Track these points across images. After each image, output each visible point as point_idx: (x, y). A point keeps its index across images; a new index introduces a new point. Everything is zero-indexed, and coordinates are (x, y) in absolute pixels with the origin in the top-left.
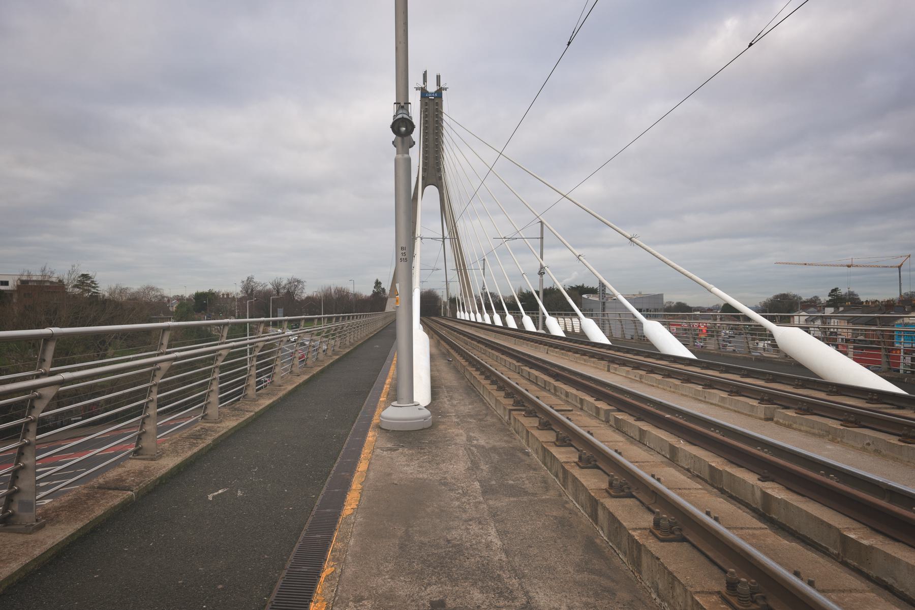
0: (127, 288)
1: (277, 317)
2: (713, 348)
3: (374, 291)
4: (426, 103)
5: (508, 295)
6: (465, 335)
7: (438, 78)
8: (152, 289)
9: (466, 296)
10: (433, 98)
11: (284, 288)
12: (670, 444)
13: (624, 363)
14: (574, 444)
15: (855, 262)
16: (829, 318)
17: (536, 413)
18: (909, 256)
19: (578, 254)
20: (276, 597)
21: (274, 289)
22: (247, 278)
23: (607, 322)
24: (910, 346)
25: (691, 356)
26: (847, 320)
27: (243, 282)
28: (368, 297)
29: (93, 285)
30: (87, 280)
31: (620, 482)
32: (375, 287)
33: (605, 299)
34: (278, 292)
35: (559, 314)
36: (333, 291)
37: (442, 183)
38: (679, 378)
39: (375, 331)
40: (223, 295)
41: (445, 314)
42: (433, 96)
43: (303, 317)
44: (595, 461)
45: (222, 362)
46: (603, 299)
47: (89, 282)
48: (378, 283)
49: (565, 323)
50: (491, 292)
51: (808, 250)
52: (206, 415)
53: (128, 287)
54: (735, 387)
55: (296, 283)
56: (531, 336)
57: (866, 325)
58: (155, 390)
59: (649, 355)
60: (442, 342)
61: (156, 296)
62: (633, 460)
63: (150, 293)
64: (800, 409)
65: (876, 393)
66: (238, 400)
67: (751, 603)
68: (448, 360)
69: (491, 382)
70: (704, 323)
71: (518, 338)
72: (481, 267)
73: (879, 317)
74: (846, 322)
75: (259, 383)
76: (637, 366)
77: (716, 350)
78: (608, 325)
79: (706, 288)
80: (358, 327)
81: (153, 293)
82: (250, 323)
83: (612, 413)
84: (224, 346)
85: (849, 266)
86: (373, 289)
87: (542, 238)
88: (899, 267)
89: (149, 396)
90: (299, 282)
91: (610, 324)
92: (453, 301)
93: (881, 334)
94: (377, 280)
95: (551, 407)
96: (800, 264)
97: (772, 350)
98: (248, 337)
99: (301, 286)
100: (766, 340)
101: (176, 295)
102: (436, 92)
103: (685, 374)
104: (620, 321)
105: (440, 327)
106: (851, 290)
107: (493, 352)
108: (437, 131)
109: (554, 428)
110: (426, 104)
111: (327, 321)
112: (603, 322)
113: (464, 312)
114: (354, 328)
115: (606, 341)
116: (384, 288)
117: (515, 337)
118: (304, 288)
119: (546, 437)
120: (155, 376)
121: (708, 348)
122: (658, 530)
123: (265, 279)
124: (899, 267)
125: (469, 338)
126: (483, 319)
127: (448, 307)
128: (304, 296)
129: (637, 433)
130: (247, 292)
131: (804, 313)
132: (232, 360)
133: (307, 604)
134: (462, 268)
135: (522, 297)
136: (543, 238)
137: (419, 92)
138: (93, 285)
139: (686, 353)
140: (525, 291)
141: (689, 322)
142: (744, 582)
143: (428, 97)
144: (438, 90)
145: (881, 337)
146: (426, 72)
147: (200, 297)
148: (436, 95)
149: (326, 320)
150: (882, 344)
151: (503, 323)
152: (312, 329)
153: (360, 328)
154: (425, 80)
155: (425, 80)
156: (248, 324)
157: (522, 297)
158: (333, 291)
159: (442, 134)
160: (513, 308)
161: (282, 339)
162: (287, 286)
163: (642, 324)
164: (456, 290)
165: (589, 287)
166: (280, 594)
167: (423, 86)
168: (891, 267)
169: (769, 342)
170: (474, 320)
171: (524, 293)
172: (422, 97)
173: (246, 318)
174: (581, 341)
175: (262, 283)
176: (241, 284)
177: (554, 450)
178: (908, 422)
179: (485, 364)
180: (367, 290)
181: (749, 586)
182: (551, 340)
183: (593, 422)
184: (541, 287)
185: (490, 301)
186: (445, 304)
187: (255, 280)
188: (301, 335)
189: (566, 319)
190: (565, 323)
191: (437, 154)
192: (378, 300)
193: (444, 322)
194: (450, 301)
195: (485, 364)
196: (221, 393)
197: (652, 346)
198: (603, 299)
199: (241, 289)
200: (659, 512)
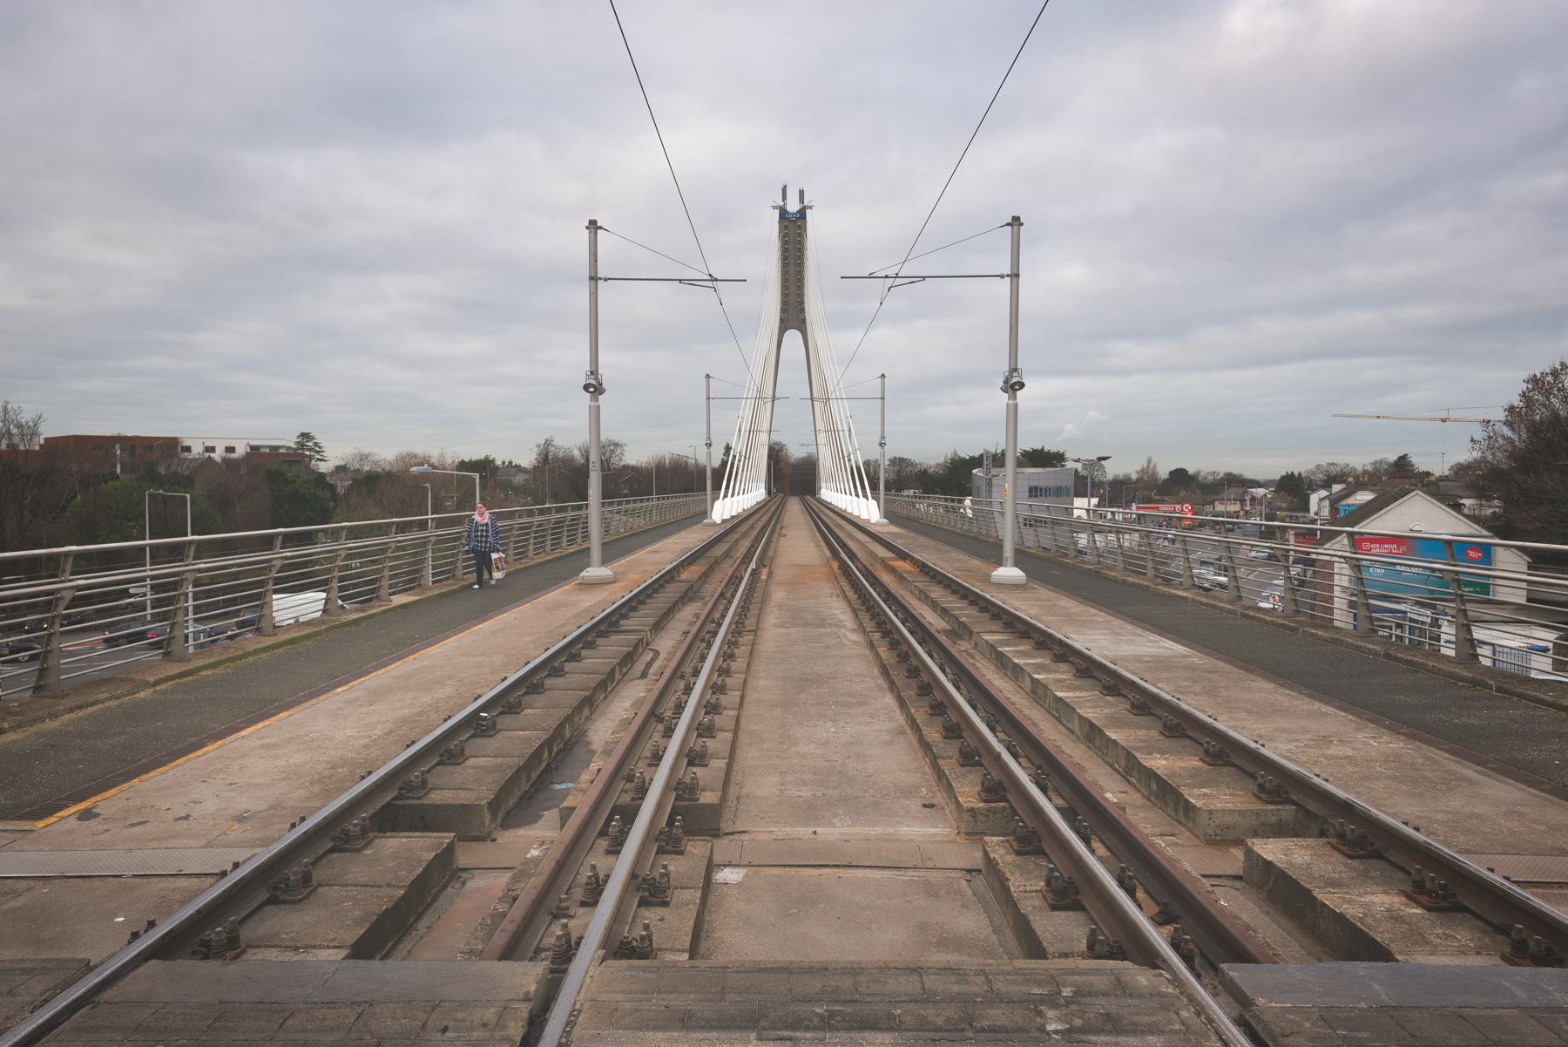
7: (802, 193)
15: (1453, 415)
21: (583, 456)
22: (544, 441)
24: (1272, 606)
27: (539, 446)
30: (308, 442)
36: (667, 461)
47: (310, 444)
53: (372, 452)
55: (612, 448)
82: (151, 546)
84: (570, 514)
85: (1444, 420)
90: (616, 445)
96: (609, 279)
98: (148, 567)
99: (619, 450)
110: (786, 227)
132: (113, 602)
136: (1017, 275)
143: (788, 218)
147: (1179, 476)
152: (272, 556)
154: (784, 198)
155: (784, 198)
156: (148, 548)
158: (667, 461)
165: (1052, 451)
167: (781, 204)
173: (187, 535)
176: (537, 449)
187: (555, 443)
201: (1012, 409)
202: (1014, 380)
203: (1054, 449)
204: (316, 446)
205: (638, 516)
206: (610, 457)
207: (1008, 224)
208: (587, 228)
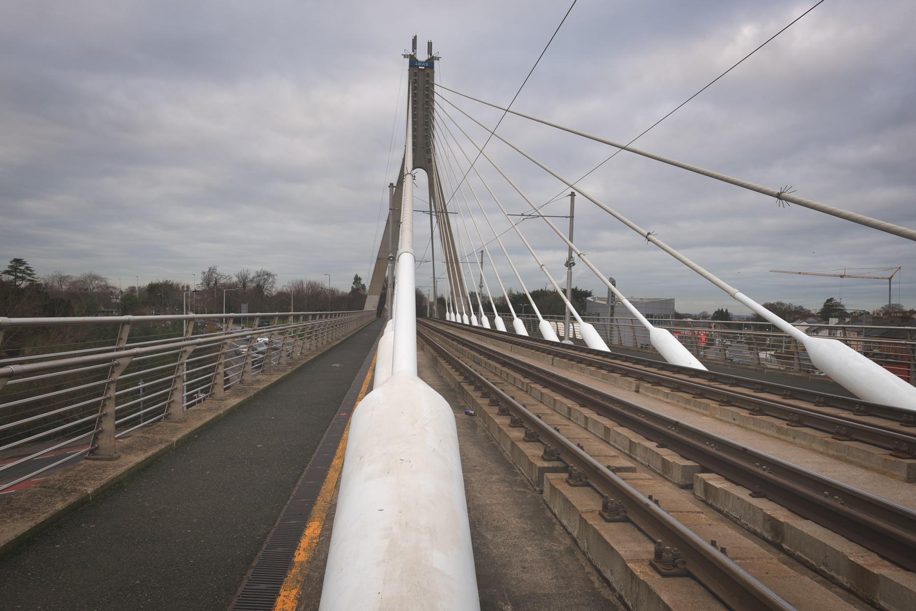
0: (68, 276)
1: (241, 313)
2: (631, 346)
3: (353, 287)
4: (416, 73)
5: (497, 296)
6: (472, 348)
7: (430, 45)
8: (96, 278)
9: (458, 296)
10: (424, 68)
11: (252, 281)
12: (605, 426)
13: (626, 373)
14: (632, 518)
15: (848, 273)
16: (834, 329)
17: (509, 411)
18: (900, 268)
19: (541, 264)
20: (246, 585)
23: (615, 329)
25: (702, 367)
26: (857, 332)
27: (204, 273)
28: (346, 294)
29: (29, 272)
30: (20, 266)
31: (616, 504)
32: (354, 283)
33: (614, 302)
34: (244, 286)
35: (551, 318)
36: (305, 286)
37: (432, 166)
38: (746, 407)
39: (344, 336)
40: (183, 287)
41: (431, 315)
42: (423, 66)
43: (277, 313)
44: (538, 436)
45: (187, 359)
46: (612, 302)
47: (22, 268)
48: (357, 279)
49: (557, 327)
50: (493, 296)
51: (794, 260)
52: (169, 414)
54: (726, 397)
55: (266, 277)
56: (523, 340)
57: (880, 337)
58: (113, 387)
59: (650, 364)
60: (443, 362)
61: (100, 286)
62: (591, 454)
63: (93, 282)
64: (791, 420)
65: (912, 414)
66: (159, 420)
67: (672, 567)
68: (467, 413)
69: (475, 388)
70: (704, 331)
71: (514, 344)
72: (478, 261)
73: (752, 324)
74: (856, 333)
75: (190, 398)
76: (641, 377)
77: (634, 348)
78: (572, 327)
79: (729, 293)
80: (332, 327)
81: (97, 282)
83: (700, 475)
84: (189, 342)
85: (842, 276)
86: (352, 285)
87: (572, 217)
88: (890, 279)
89: (106, 394)
90: (269, 275)
91: (619, 331)
92: (441, 301)
93: (911, 349)
94: (356, 276)
95: (538, 416)
96: (795, 273)
97: (776, 362)
98: (292, 323)
99: (271, 279)
100: (769, 350)
101: (132, 286)
102: (426, 61)
103: (794, 413)
104: (633, 328)
105: (429, 332)
106: (894, 301)
107: (546, 391)
108: (427, 107)
109: (541, 439)
111: (303, 319)
112: (612, 328)
113: (455, 314)
114: (328, 328)
115: (605, 348)
116: (364, 285)
117: (511, 343)
118: (274, 282)
119: (517, 434)
120: (114, 372)
121: (708, 358)
122: (659, 562)
123: (229, 272)
124: (890, 279)
125: (445, 337)
126: (479, 321)
127: (435, 308)
128: (274, 292)
129: (659, 464)
130: (208, 285)
131: (804, 323)
133: (275, 598)
134: (453, 261)
135: (512, 299)
136: (573, 217)
137: (407, 60)
138: (29, 272)
139: (698, 365)
140: (515, 293)
141: (694, 330)
142: (612, 501)
144: (429, 59)
145: (911, 352)
146: (415, 37)
147: (153, 289)
148: (427, 64)
149: (232, 321)
150: (755, 344)
151: (507, 329)
152: (298, 325)
153: (335, 327)
157: (512, 299)
158: (305, 286)
159: (433, 118)
160: (503, 310)
161: (225, 341)
162: (255, 280)
163: (649, 331)
164: (445, 289)
166: (255, 573)
167: (412, 54)
168: (882, 278)
169: (773, 353)
170: (460, 322)
171: (514, 295)
172: (410, 66)
173: (223, 313)
174: (649, 362)
175: (226, 275)
177: (522, 446)
178: (845, 423)
179: (470, 368)
180: (345, 287)
181: (672, 553)
182: (542, 345)
183: (584, 434)
184: (569, 286)
185: (478, 302)
186: (432, 305)
187: (217, 272)
188: (255, 336)
189: (558, 323)
190: (557, 327)
191: (426, 133)
192: (356, 297)
193: (432, 324)
194: (437, 301)
195: (470, 368)
196: (117, 419)
197: (659, 356)
198: (612, 302)
199: (202, 281)
200: (660, 542)
201: (569, 273)
202: (571, 262)
203: (584, 289)
204: (28, 270)
205: (309, 338)
206: (264, 284)
207: (570, 195)
208: (389, 187)
